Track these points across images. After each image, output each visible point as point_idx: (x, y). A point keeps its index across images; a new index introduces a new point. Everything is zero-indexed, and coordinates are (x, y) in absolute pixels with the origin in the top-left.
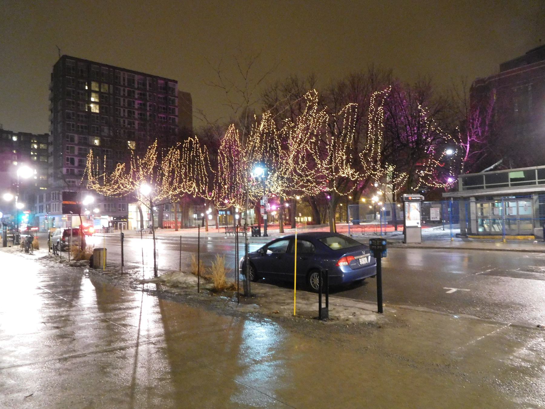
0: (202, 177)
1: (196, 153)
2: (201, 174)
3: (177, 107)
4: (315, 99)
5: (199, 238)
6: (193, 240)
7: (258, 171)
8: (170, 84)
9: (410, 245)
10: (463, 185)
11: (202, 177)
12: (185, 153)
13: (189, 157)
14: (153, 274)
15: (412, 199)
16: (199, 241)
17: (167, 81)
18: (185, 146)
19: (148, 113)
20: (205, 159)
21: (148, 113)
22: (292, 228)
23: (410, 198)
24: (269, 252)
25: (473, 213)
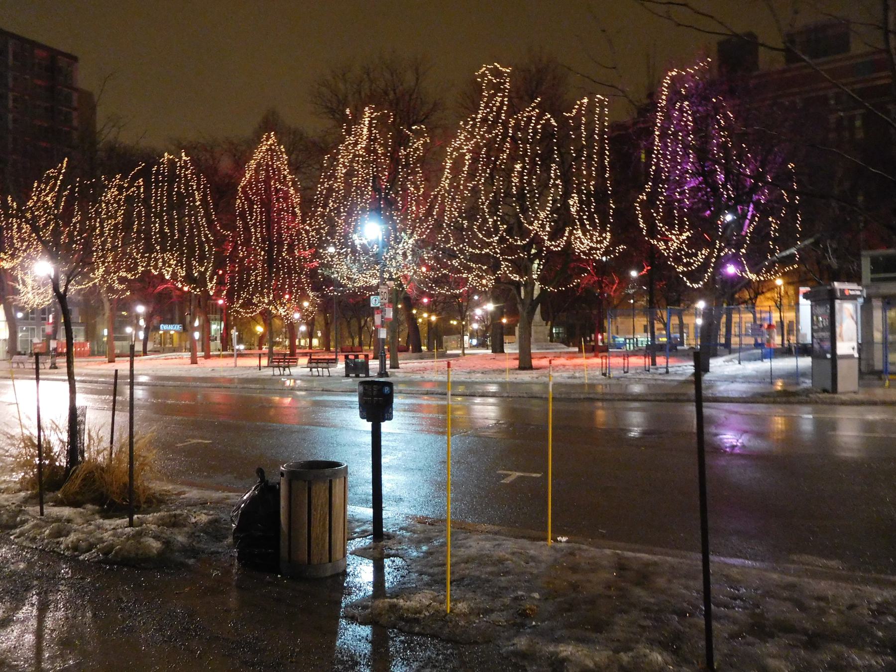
0: (201, 244)
1: (186, 189)
2: (199, 236)
3: (75, 109)
4: (505, 83)
5: (38, 379)
6: (55, 377)
7: (370, 231)
8: (62, 62)
9: (844, 398)
10: (873, 272)
11: (201, 244)
12: (157, 188)
13: (170, 196)
14: (313, 488)
15: (850, 295)
16: (115, 384)
17: (54, 54)
18: (158, 170)
19: (10, 116)
20: (204, 200)
21: (10, 116)
22: (110, 362)
23: (847, 293)
24: (601, 415)
25: (878, 330)
